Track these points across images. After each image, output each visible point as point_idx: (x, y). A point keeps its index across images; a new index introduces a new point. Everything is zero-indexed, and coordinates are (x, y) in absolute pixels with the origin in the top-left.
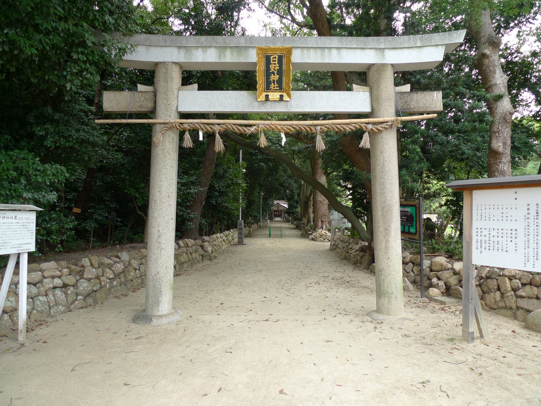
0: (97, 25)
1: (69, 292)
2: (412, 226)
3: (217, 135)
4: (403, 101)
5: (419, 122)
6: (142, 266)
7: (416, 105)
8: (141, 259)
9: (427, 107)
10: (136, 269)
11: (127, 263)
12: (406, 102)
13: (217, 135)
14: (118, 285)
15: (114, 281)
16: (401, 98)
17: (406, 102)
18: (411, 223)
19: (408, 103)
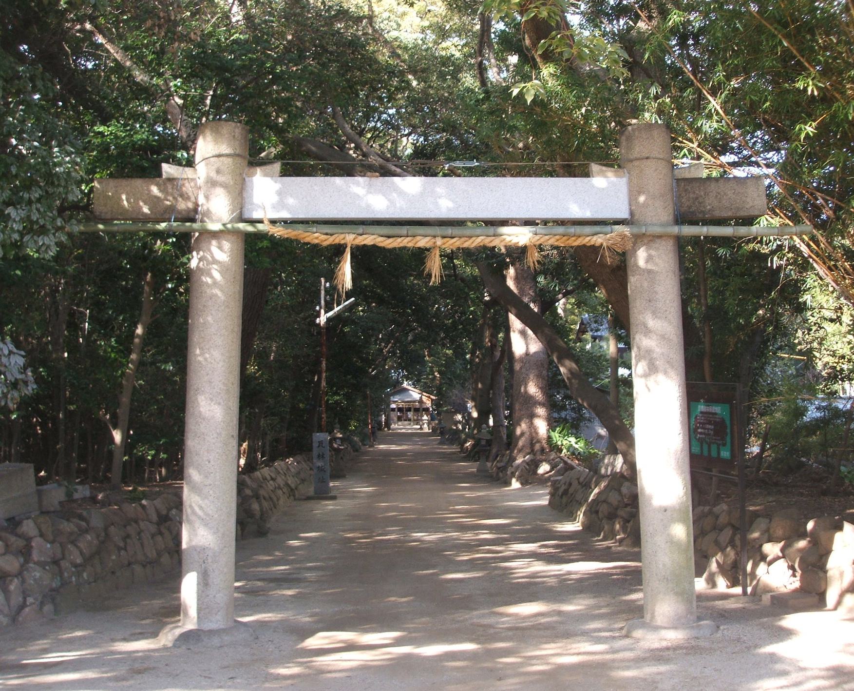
0: (703, 308)
1: (12, 587)
2: (724, 445)
3: (348, 250)
4: (692, 196)
5: (420, 255)
6: (128, 541)
7: (716, 204)
8: (125, 526)
9: (738, 209)
10: (120, 549)
11: (103, 534)
12: (697, 198)
13: (348, 250)
14: (91, 580)
15: (84, 571)
16: (686, 190)
17: (697, 198)
18: (723, 439)
19: (701, 200)
